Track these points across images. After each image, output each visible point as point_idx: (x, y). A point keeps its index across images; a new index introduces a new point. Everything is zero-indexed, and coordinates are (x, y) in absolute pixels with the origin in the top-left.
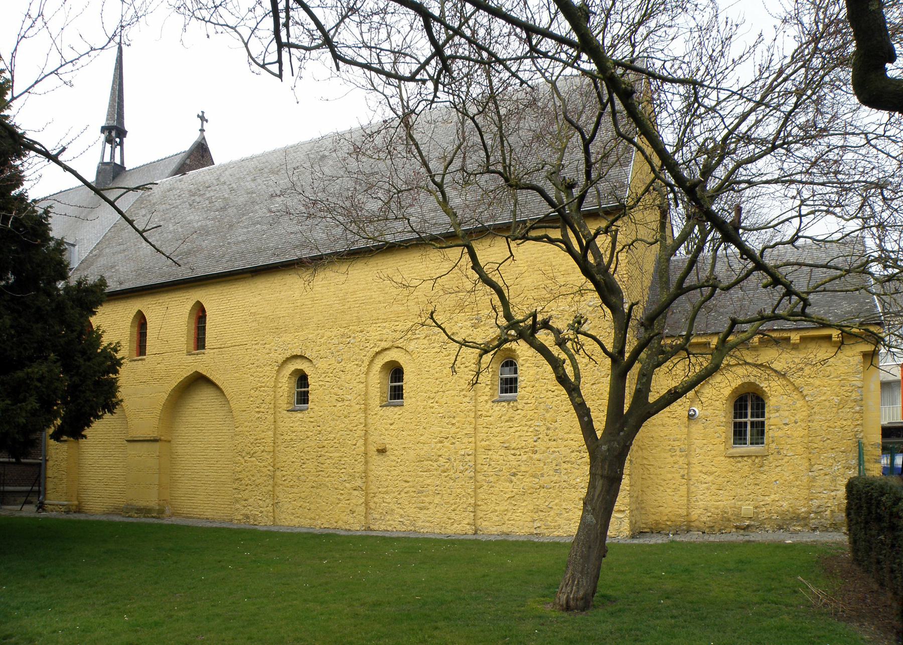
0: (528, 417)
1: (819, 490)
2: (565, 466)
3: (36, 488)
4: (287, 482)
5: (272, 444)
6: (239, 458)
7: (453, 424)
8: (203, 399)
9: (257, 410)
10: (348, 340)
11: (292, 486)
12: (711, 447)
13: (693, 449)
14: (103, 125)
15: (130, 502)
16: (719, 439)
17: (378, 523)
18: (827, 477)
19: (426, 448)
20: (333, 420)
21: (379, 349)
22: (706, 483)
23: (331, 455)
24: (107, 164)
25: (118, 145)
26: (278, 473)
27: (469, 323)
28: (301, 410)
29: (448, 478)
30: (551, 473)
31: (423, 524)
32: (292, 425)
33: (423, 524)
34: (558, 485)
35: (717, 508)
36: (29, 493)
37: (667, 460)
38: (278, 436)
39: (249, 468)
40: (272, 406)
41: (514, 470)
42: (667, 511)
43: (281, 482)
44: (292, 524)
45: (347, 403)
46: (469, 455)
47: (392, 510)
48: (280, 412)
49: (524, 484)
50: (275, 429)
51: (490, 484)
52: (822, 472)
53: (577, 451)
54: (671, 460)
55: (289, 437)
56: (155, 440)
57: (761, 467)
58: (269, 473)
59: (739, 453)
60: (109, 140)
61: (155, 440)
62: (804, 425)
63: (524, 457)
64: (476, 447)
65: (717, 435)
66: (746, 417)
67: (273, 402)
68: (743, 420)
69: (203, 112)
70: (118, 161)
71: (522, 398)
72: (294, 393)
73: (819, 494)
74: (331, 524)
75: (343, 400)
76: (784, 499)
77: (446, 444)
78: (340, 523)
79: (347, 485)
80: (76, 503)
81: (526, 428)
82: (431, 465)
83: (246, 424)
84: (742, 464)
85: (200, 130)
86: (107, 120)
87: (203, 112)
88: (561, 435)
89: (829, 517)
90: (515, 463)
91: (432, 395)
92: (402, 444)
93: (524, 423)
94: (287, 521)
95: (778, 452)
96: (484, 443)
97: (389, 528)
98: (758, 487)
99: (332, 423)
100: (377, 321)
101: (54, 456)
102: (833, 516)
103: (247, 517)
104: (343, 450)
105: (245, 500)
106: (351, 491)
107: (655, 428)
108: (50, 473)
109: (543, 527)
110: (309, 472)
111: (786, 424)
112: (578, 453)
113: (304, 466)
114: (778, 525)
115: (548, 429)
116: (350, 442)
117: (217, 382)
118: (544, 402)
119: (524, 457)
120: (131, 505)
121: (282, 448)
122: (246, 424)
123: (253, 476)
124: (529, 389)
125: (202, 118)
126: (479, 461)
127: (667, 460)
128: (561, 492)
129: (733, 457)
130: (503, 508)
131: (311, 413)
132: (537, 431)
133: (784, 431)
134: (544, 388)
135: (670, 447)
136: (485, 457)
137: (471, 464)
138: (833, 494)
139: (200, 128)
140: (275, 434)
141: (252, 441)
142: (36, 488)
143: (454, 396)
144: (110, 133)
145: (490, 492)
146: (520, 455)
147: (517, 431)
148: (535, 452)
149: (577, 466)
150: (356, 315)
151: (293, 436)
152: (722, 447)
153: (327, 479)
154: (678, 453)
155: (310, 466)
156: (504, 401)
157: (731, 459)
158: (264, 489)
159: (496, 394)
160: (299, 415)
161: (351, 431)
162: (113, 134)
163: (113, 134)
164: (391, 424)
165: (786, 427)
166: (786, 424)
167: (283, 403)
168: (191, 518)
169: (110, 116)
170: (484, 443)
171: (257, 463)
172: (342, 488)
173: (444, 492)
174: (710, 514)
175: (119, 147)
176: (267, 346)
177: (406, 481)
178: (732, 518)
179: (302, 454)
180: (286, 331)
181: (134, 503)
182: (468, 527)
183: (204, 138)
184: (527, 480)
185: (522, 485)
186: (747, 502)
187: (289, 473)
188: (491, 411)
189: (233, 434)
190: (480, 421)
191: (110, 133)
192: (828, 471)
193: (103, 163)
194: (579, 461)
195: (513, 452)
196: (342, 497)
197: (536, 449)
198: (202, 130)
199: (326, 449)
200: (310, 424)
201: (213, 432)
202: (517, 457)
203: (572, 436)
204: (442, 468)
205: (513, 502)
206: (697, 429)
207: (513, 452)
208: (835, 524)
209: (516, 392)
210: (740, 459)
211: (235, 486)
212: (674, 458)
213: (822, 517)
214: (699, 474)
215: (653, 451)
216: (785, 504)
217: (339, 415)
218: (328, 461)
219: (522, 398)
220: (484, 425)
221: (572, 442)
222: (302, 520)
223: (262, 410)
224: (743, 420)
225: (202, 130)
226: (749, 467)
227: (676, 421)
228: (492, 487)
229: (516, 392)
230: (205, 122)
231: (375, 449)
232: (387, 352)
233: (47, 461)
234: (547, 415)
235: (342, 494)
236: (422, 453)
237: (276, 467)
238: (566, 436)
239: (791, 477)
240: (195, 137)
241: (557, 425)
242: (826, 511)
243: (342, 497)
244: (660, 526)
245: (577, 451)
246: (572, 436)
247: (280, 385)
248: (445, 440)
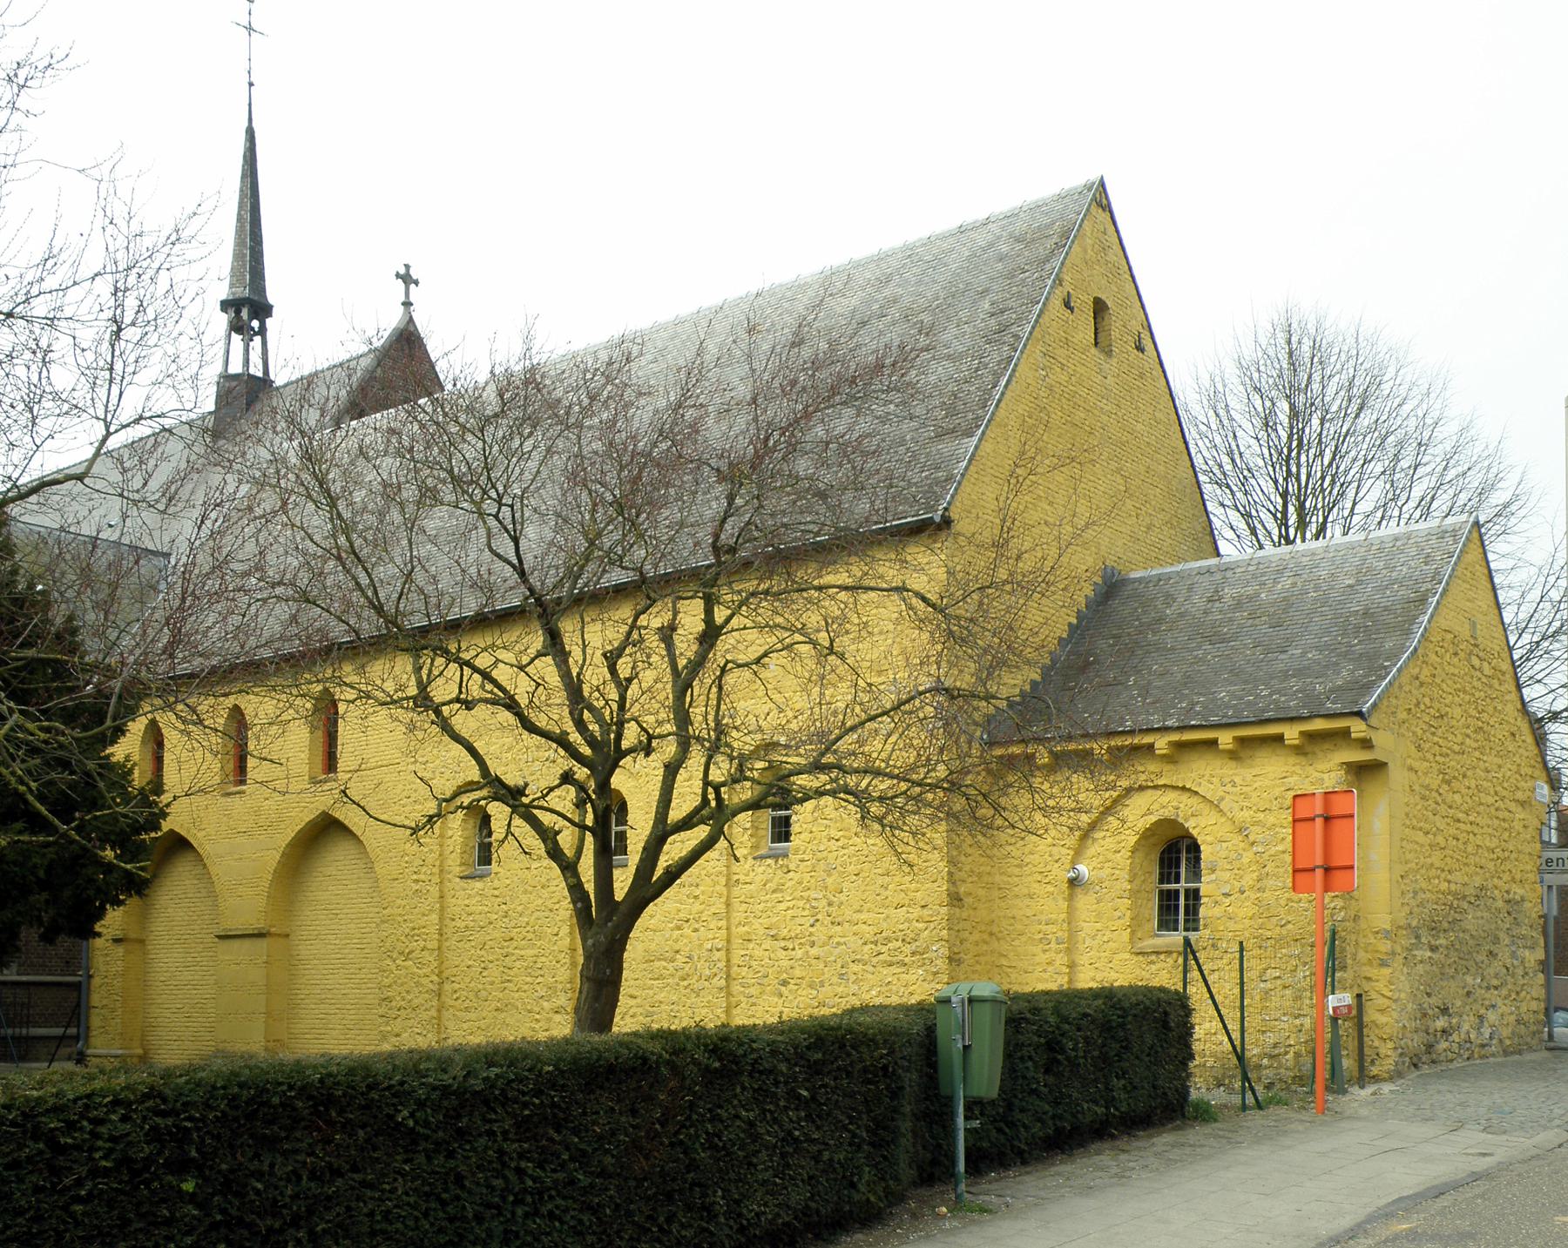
2: (855, 968)
3: (72, 1031)
5: (436, 936)
6: (388, 962)
7: (696, 897)
8: (336, 862)
9: (415, 877)
12: (1108, 935)
13: (1080, 939)
14: (224, 297)
15: (221, 1046)
16: (1122, 921)
18: (1287, 992)
19: (658, 937)
20: (525, 892)
23: (523, 953)
24: (236, 377)
25: (256, 334)
26: (447, 987)
28: (481, 877)
30: (835, 979)
32: (467, 902)
36: (61, 1039)
37: (1037, 959)
38: (447, 922)
40: (435, 870)
41: (785, 976)
43: (452, 1003)
46: (718, 950)
48: (450, 881)
49: (799, 999)
50: (442, 909)
51: (751, 1000)
52: (1279, 982)
54: (1043, 958)
55: (464, 924)
56: (260, 935)
58: (431, 985)
59: (1154, 946)
60: (237, 327)
61: (260, 935)
62: (1253, 896)
64: (729, 935)
65: (1118, 914)
66: (1177, 881)
67: (438, 863)
68: (1173, 886)
69: (407, 267)
70: (256, 370)
71: (796, 851)
77: (687, 931)
79: (545, 1004)
80: (140, 1051)
81: (801, 903)
82: (665, 968)
83: (399, 901)
84: (1158, 966)
85: (403, 304)
86: (232, 285)
87: (407, 267)
89: (1291, 1064)
90: (785, 963)
93: (798, 894)
95: (1213, 946)
96: (742, 930)
99: (524, 898)
101: (102, 968)
102: (1297, 1063)
105: (397, 1035)
107: (1017, 902)
108: (96, 999)
110: (492, 983)
111: (1227, 895)
114: (1216, 1078)
115: (830, 904)
116: (549, 931)
117: (354, 829)
118: (825, 859)
119: (799, 953)
121: (452, 942)
122: (399, 901)
123: (408, 992)
124: (805, 836)
125: (407, 279)
126: (735, 960)
127: (1037, 959)
132: (814, 908)
133: (1223, 908)
134: (824, 834)
135: (1041, 935)
136: (743, 952)
137: (722, 965)
138: (1297, 1022)
139: (403, 299)
140: (441, 919)
141: (407, 931)
142: (72, 1031)
144: (238, 312)
146: (793, 949)
147: (788, 908)
148: (813, 944)
149: (871, 969)
152: (1126, 935)
153: (516, 995)
154: (1053, 945)
155: (494, 972)
157: (1140, 958)
158: (425, 1015)
159: (763, 843)
160: (478, 885)
161: (551, 910)
162: (245, 314)
163: (245, 314)
165: (1227, 901)
166: (1227, 895)
167: (454, 864)
169: (236, 274)
170: (742, 930)
172: (537, 1009)
175: (258, 339)
179: (483, 952)
183: (411, 320)
184: (804, 993)
187: (462, 986)
188: (752, 874)
189: (378, 920)
190: (736, 891)
191: (238, 312)
192: (1288, 980)
193: (226, 377)
194: (875, 960)
195: (783, 944)
197: (813, 938)
198: (407, 304)
199: (515, 944)
200: (493, 899)
201: (353, 916)
203: (863, 916)
204: (680, 973)
206: (1084, 902)
207: (783, 944)
208: (1301, 1078)
209: (787, 840)
210: (1153, 957)
211: (381, 1011)
212: (1048, 955)
215: (1016, 943)
217: (533, 884)
218: (518, 963)
219: (796, 851)
221: (864, 926)
223: (422, 877)
224: (1173, 886)
225: (407, 304)
226: (1169, 972)
227: (1050, 888)
228: (754, 1004)
229: (787, 840)
230: (412, 286)
233: (90, 977)
234: (830, 880)
236: (653, 946)
237: (445, 975)
238: (856, 916)
240: (391, 320)
241: (843, 897)
242: (1286, 1053)
246: (863, 916)
247: (450, 833)
248: (686, 925)
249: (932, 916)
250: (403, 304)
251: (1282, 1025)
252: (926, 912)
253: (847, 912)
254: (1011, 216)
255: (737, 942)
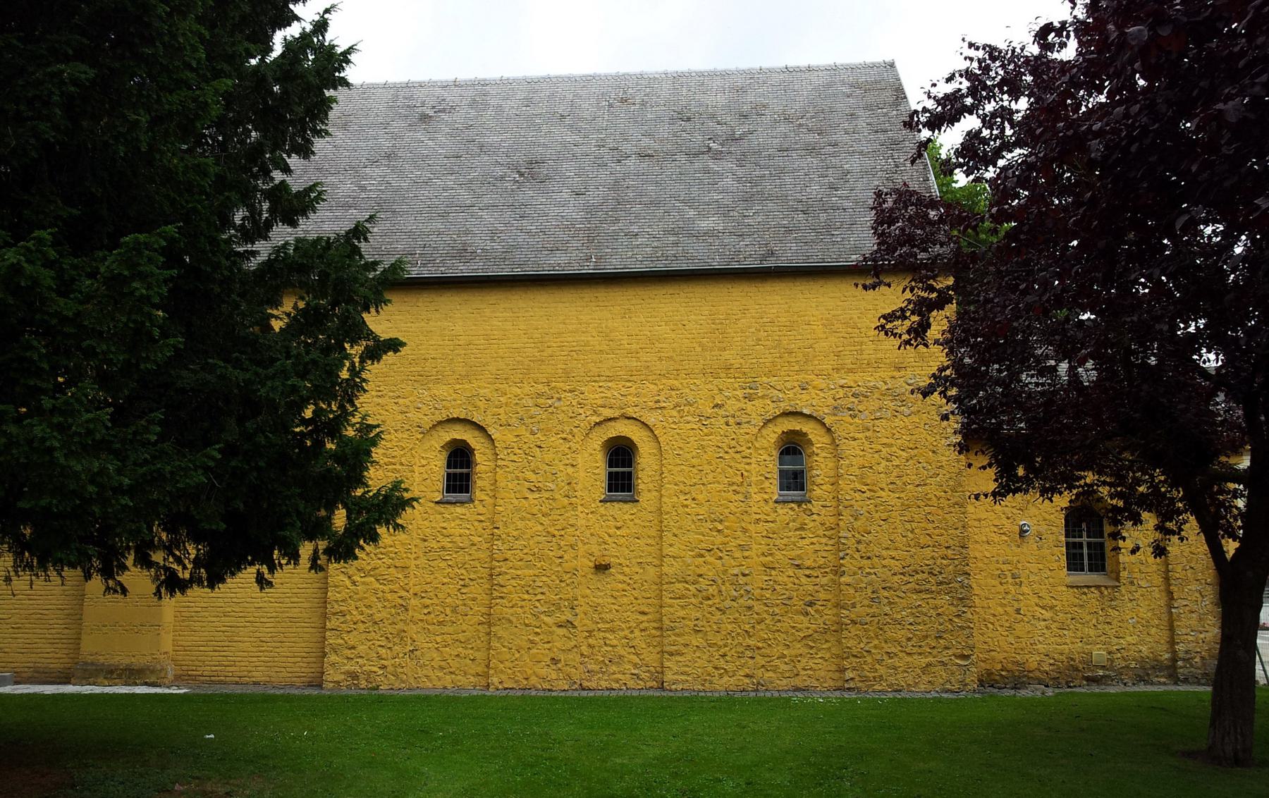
0: (828, 524)
1: (1184, 631)
4: (432, 616)
7: (719, 531)
10: (550, 402)
11: (440, 623)
17: (596, 677)
21: (602, 418)
22: (1045, 620)
23: (519, 572)
27: (740, 393)
29: (714, 608)
30: (866, 602)
31: (676, 677)
33: (676, 677)
34: (876, 619)
35: (1062, 654)
39: (361, 595)
42: (1000, 657)
44: (439, 684)
45: (547, 495)
47: (621, 657)
52: (1187, 608)
53: (901, 574)
57: (1112, 600)
63: (824, 581)
68: (1077, 540)
72: (443, 476)
73: (1186, 637)
74: (516, 682)
75: (539, 489)
76: (1142, 642)
78: (534, 680)
79: (546, 619)
88: (877, 551)
89: (1199, 664)
91: (687, 489)
92: (636, 558)
94: (430, 681)
97: (615, 686)
98: (1110, 627)
99: (520, 524)
100: (597, 379)
102: (1204, 664)
103: (354, 676)
104: (539, 565)
106: (555, 628)
109: (857, 679)
110: (474, 599)
112: (902, 577)
113: (464, 591)
120: (92, 664)
128: (881, 629)
129: (1077, 587)
130: (794, 652)
131: (481, 507)
136: (767, 578)
138: (1202, 636)
143: (719, 491)
145: (775, 628)
150: (564, 367)
151: (445, 542)
156: (792, 502)
160: (459, 510)
164: (618, 528)
168: (221, 682)
171: (378, 586)
173: (709, 629)
174: (1052, 661)
176: (401, 401)
177: (643, 613)
178: (1081, 666)
180: (437, 381)
181: (101, 659)
182: (747, 680)
185: (823, 619)
186: (1098, 646)
187: (435, 601)
194: (904, 588)
195: (807, 572)
196: (537, 639)
202: (813, 579)
205: (810, 643)
210: (1086, 590)
213: (1192, 666)
214: (1036, 608)
216: (1144, 649)
220: (764, 534)
221: (893, 561)
222: (459, 677)
231: (592, 565)
232: (612, 424)
235: (537, 634)
239: (1149, 614)
243: (537, 639)
244: (993, 677)
245: (901, 574)
249: (955, 554)
251: (1191, 638)
252: (950, 552)
253: (876, 549)
254: (852, 68)
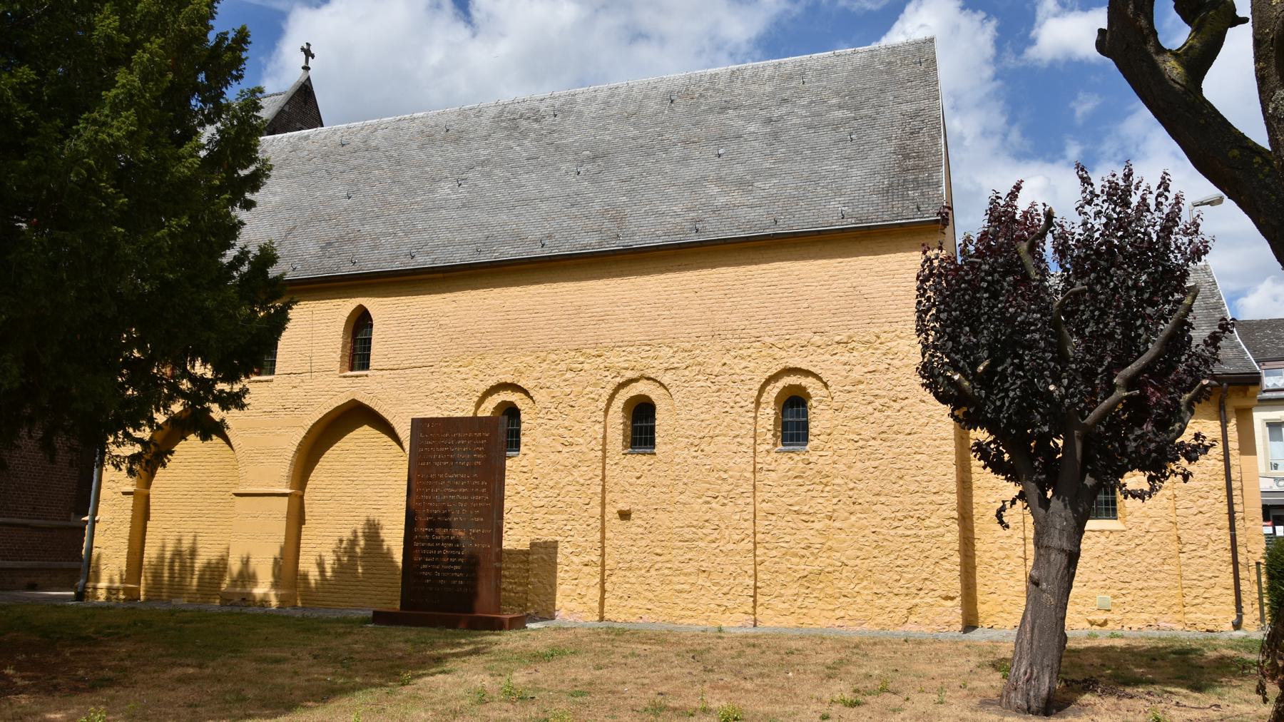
7: (724, 479)
23: (552, 517)
46: (746, 520)
82: (694, 533)
85: (303, 68)
125: (308, 53)
126: (760, 528)
137: (750, 532)
139: (303, 64)
147: (809, 490)
198: (306, 68)
204: (709, 538)
218: (547, 525)
250: (303, 68)
255: (760, 514)
